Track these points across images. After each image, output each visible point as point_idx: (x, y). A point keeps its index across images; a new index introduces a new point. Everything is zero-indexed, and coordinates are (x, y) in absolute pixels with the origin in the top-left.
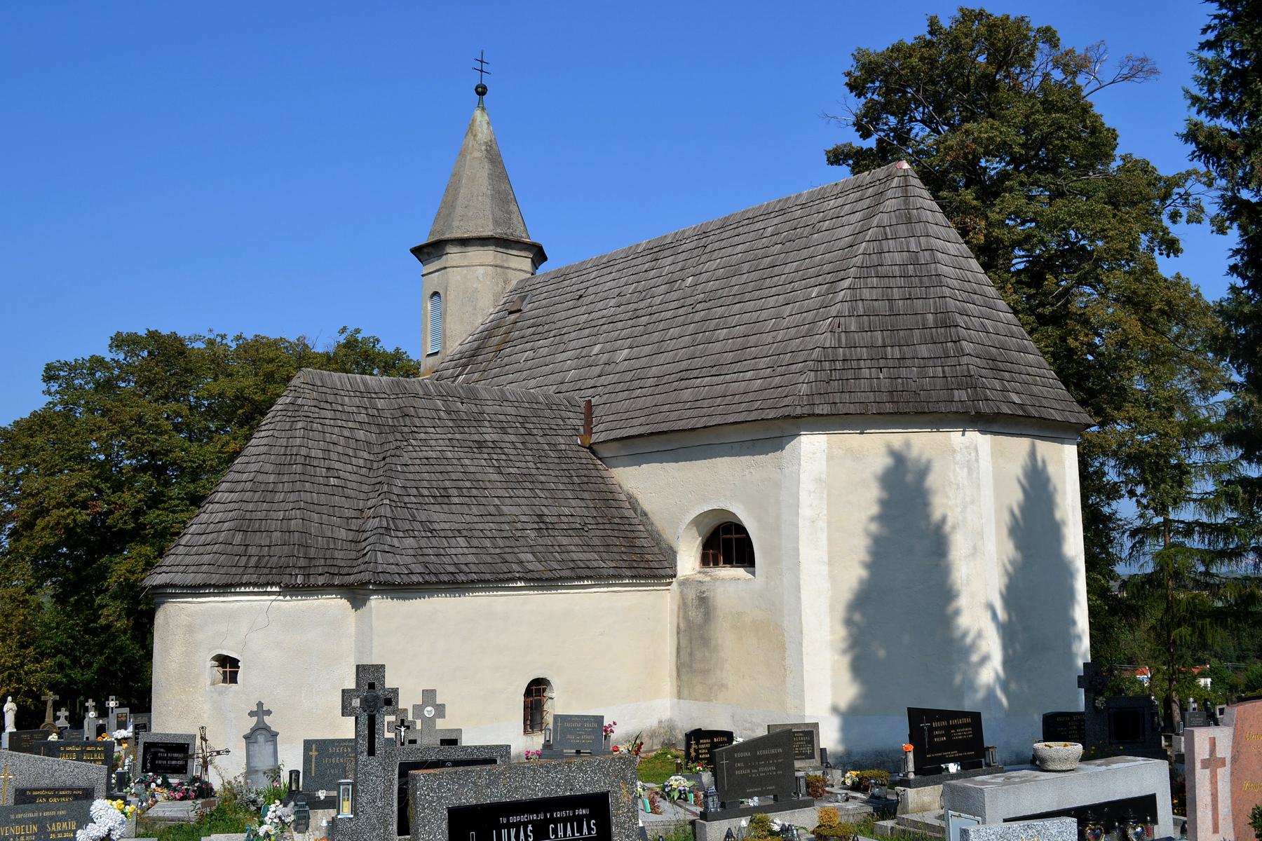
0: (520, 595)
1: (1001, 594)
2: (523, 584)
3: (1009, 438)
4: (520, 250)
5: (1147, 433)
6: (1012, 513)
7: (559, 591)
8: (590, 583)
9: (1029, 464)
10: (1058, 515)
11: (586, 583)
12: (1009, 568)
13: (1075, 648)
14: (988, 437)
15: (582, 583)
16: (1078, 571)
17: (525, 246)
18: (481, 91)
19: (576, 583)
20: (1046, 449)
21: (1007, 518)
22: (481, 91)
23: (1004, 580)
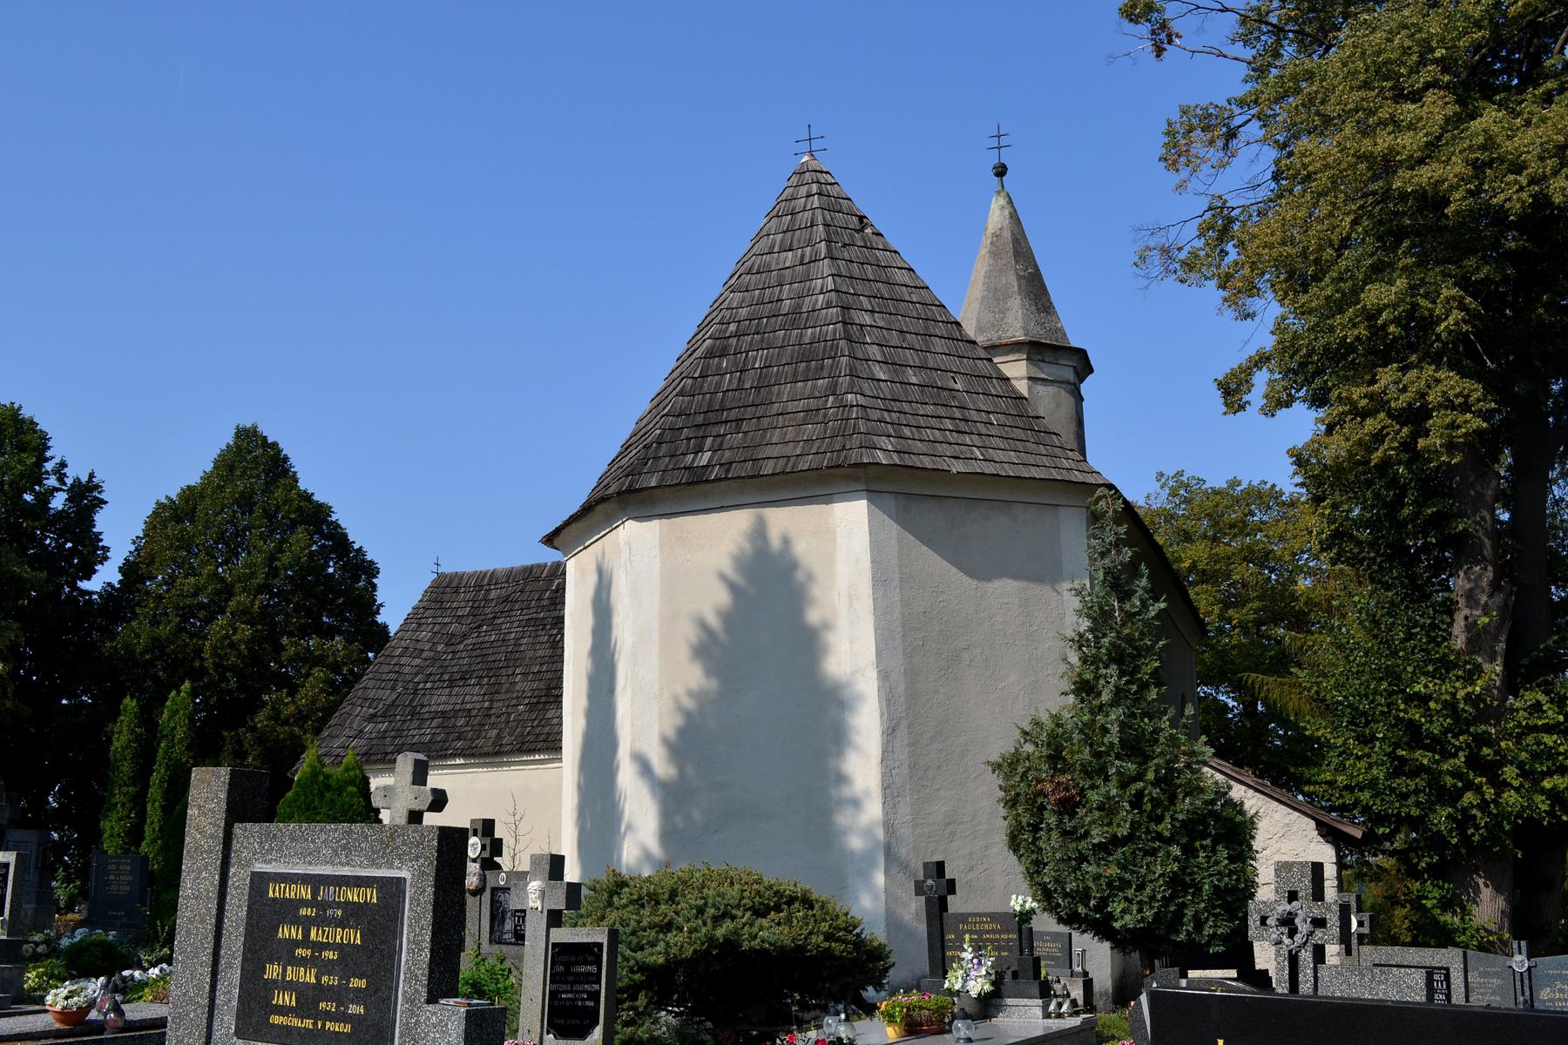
0: (447, 774)
1: (665, 741)
2: (462, 761)
3: (700, 517)
4: (1006, 354)
5: (222, 511)
6: (703, 625)
7: (512, 768)
8: (542, 757)
9: (747, 547)
10: (813, 616)
11: (537, 757)
12: (689, 703)
13: (843, 819)
14: (655, 525)
15: (532, 758)
16: (860, 697)
17: (1008, 348)
18: (1001, 171)
19: (525, 758)
20: (784, 521)
21: (690, 633)
22: (1001, 171)
23: (679, 720)
